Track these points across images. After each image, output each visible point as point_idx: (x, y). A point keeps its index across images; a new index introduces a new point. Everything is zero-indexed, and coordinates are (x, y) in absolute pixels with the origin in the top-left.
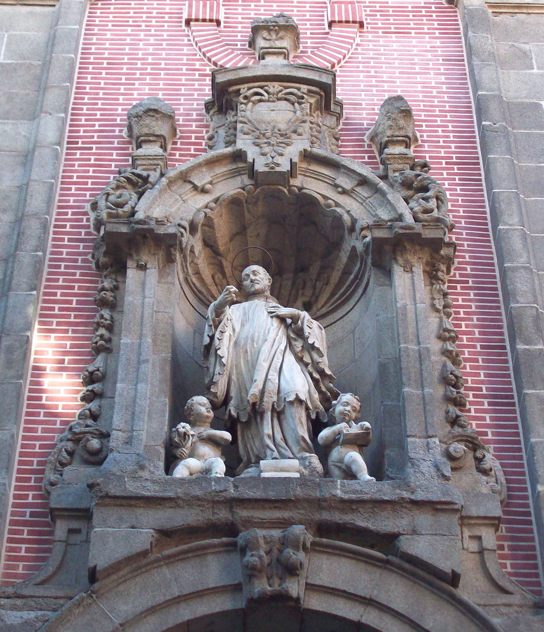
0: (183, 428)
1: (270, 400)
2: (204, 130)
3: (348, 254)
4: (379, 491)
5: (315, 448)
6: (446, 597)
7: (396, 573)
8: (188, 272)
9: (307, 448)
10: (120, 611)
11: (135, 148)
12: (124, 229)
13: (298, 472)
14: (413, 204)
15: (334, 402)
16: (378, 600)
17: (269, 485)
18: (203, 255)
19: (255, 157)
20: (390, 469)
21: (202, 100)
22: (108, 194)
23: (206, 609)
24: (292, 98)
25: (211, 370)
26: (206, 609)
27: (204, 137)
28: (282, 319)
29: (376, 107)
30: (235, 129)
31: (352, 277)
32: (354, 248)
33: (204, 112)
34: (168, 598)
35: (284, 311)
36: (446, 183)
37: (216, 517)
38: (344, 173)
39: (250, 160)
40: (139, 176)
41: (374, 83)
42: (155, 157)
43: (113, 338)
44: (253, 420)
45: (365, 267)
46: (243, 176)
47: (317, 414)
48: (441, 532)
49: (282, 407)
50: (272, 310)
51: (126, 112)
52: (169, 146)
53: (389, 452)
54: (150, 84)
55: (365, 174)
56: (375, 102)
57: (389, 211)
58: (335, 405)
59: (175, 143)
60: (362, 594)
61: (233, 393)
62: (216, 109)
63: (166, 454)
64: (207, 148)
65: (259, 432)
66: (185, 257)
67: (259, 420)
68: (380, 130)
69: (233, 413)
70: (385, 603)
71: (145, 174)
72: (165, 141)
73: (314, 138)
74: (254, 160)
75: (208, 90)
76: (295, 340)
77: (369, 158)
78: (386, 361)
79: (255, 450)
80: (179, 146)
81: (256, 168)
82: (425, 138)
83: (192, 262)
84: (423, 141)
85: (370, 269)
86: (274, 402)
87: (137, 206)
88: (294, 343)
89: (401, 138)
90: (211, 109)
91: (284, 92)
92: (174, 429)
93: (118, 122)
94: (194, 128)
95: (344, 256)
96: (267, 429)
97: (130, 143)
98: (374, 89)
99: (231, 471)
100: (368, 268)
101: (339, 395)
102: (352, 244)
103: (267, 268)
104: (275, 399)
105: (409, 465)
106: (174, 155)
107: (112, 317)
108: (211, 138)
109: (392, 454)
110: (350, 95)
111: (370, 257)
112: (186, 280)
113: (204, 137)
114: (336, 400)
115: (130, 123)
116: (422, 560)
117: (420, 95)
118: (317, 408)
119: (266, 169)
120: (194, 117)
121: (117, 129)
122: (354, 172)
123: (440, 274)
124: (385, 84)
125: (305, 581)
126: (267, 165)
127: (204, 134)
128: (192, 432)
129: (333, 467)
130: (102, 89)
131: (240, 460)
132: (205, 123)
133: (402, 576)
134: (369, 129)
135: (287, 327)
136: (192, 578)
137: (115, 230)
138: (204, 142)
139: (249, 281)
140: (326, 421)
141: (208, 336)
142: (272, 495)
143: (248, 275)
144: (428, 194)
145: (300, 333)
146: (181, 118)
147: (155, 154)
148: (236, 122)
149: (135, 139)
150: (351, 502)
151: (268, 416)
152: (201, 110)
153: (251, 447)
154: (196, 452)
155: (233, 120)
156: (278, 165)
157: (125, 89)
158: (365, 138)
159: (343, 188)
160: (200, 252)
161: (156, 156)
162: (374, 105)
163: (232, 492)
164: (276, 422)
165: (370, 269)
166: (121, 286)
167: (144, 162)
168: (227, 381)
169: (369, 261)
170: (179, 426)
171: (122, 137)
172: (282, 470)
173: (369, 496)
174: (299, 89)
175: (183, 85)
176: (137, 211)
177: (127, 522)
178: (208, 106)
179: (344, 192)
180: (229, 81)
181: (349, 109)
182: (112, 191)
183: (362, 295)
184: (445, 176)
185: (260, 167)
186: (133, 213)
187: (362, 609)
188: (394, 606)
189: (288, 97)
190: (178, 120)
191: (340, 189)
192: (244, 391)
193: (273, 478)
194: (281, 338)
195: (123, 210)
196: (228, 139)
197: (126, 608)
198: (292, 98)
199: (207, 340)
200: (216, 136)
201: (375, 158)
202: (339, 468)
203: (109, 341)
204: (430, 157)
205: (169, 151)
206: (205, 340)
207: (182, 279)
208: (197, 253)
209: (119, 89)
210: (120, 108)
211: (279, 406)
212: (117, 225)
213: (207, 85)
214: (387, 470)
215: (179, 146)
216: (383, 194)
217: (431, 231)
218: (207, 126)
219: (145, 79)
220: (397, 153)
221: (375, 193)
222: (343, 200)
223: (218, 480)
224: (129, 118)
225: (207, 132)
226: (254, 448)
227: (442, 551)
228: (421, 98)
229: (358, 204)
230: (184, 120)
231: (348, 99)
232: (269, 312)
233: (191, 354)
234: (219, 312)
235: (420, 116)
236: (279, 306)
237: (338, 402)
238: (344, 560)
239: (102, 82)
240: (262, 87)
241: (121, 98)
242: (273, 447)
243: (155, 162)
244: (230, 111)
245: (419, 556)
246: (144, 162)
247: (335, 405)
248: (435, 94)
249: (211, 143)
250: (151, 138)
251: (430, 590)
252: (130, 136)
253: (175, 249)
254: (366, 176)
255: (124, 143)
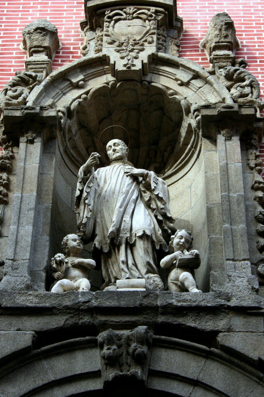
0: (59, 257)
1: (125, 235)
2: (80, 42)
3: (186, 130)
4: (203, 300)
5: (158, 271)
6: (255, 379)
7: (217, 361)
8: (67, 146)
9: (151, 270)
10: (9, 393)
11: (28, 56)
12: (18, 114)
13: (145, 287)
14: (233, 91)
15: (172, 236)
16: (203, 381)
17: (121, 297)
18: (79, 133)
19: (116, 60)
20: (214, 285)
21: (78, 21)
22: (6, 90)
23: (74, 390)
24: (144, 16)
25: (81, 215)
26: (74, 390)
27: (79, 47)
28: (135, 178)
29: (208, 23)
30: (102, 40)
31: (189, 146)
32: (190, 125)
33: (80, 29)
34: (45, 382)
35: (136, 171)
36: (260, 76)
37: (81, 321)
38: (182, 70)
39: (112, 62)
40: (30, 76)
41: (207, 5)
42: (43, 63)
43: (9, 193)
44: (113, 251)
45: (198, 139)
46: (107, 75)
47: (161, 245)
48: (250, 330)
49: (133, 241)
50: (128, 171)
51: (21, 31)
52: (54, 55)
53: (213, 272)
54: (41, 11)
55: (198, 70)
56: (208, 18)
57: (216, 97)
58: (173, 238)
59: (58, 53)
60: (191, 377)
61: (97, 232)
62: (88, 27)
63: (47, 277)
64: (82, 55)
65: (117, 259)
66: (64, 134)
67: (117, 251)
68: (209, 38)
69: (97, 246)
70: (209, 384)
71: (34, 74)
72: (50, 51)
73: (160, 46)
74: (115, 62)
75: (83, 14)
76: (145, 192)
77: (203, 59)
78: (212, 206)
79: (114, 273)
80: (61, 54)
81: (116, 68)
82: (245, 44)
83: (70, 139)
84: (243, 46)
85: (201, 140)
86: (127, 237)
87: (28, 98)
88: (144, 194)
89: (225, 44)
90: (85, 27)
91: (138, 12)
92: (53, 258)
93: (17, 38)
94: (72, 41)
95: (183, 132)
96: (122, 257)
97: (25, 53)
98: (207, 9)
99: (94, 287)
100: (200, 139)
101: (176, 231)
102: (188, 122)
103: (126, 142)
104: (128, 235)
105: (228, 280)
106: (58, 61)
107: (8, 178)
108: (85, 48)
109: (215, 273)
110: (189, 14)
111: (201, 131)
112: (66, 151)
113: (79, 47)
114: (174, 235)
115: (24, 38)
116: (236, 351)
117: (242, 12)
118: (161, 242)
119: (125, 69)
120: (73, 33)
121: (16, 44)
122: (189, 69)
123: (253, 141)
124: (215, 6)
125: (148, 367)
126: (125, 65)
127: (80, 45)
128: (66, 260)
129: (171, 284)
130: (5, 15)
131: (103, 281)
132: (80, 37)
133: (222, 363)
134: (202, 38)
135: (138, 183)
136: (63, 368)
137: (10, 115)
138: (79, 51)
139: (112, 150)
140: (167, 251)
141: (79, 189)
142: (123, 303)
143: (110, 146)
144: (244, 83)
145: (148, 187)
146: (63, 34)
147: (42, 60)
148: (102, 36)
149: (28, 50)
150: (182, 308)
151: (123, 248)
152: (77, 28)
153: (111, 271)
154: (69, 275)
155: (100, 34)
156: (134, 65)
157: (22, 15)
158: (199, 45)
159: (182, 81)
160: (76, 132)
161: (43, 61)
162: (206, 21)
163: (94, 303)
164: (129, 252)
165: (201, 140)
166: (16, 155)
167: (34, 66)
168: (93, 223)
169: (200, 134)
170: (56, 256)
171: (19, 49)
172: (132, 286)
173: (196, 303)
174: (149, 10)
175: (65, 10)
176: (28, 101)
177: (15, 326)
178: (83, 25)
179: (182, 84)
180: (97, 5)
181: (188, 24)
182: (9, 88)
183: (196, 159)
184: (259, 71)
185: (120, 66)
186: (25, 102)
187: (192, 388)
188: (215, 386)
189: (140, 16)
190: (61, 36)
191: (179, 82)
192: (105, 230)
193: (125, 291)
194: (133, 191)
195: (18, 100)
196: (97, 48)
197: (13, 391)
198: (144, 16)
199: (78, 193)
200: (88, 47)
201: (206, 59)
202: (176, 284)
203: (6, 195)
204: (248, 58)
205: (53, 58)
206: (77, 193)
207: (62, 150)
208: (74, 132)
209: (18, 15)
210: (18, 28)
211: (131, 241)
212: (12, 111)
213: (82, 10)
214: (212, 285)
215: (61, 54)
216: (211, 84)
217: (245, 109)
218: (82, 40)
219: (37, 7)
220: (222, 54)
221: (205, 84)
222: (183, 90)
223: (83, 294)
224: (23, 35)
225: (82, 44)
226: (114, 272)
227: (251, 344)
228: (242, 15)
229: (193, 92)
230: (65, 36)
231: (187, 17)
232: (125, 173)
233: (70, 205)
234: (88, 172)
235: (241, 27)
236: (134, 168)
237: (176, 236)
238: (177, 352)
239: (5, 10)
240: (122, 10)
241: (19, 21)
242: (126, 270)
243: (43, 66)
244: (99, 28)
245: (234, 348)
246: (34, 66)
247: (173, 238)
248: (252, 11)
249: (84, 52)
250: (39, 49)
251: (243, 374)
252: (25, 48)
253: (56, 129)
254: (198, 72)
255: (21, 53)
